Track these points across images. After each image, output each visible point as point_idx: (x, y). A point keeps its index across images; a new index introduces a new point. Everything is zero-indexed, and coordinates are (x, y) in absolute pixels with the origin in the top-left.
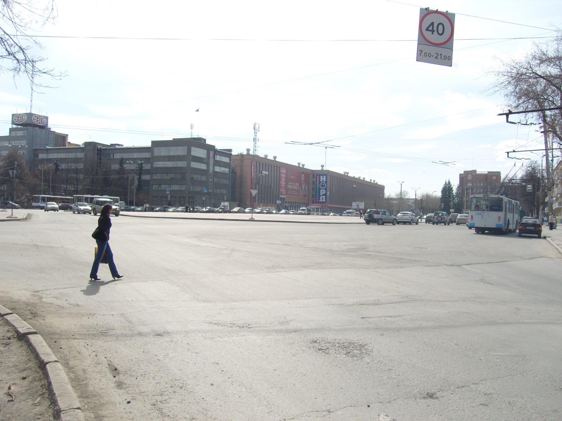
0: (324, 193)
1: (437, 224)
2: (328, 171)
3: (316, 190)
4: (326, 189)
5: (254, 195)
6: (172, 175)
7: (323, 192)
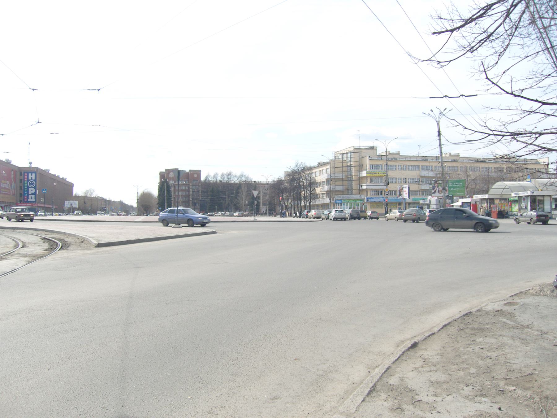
0: (34, 191)
1: (418, 222)
3: (24, 188)
4: (35, 188)
5: (255, 196)
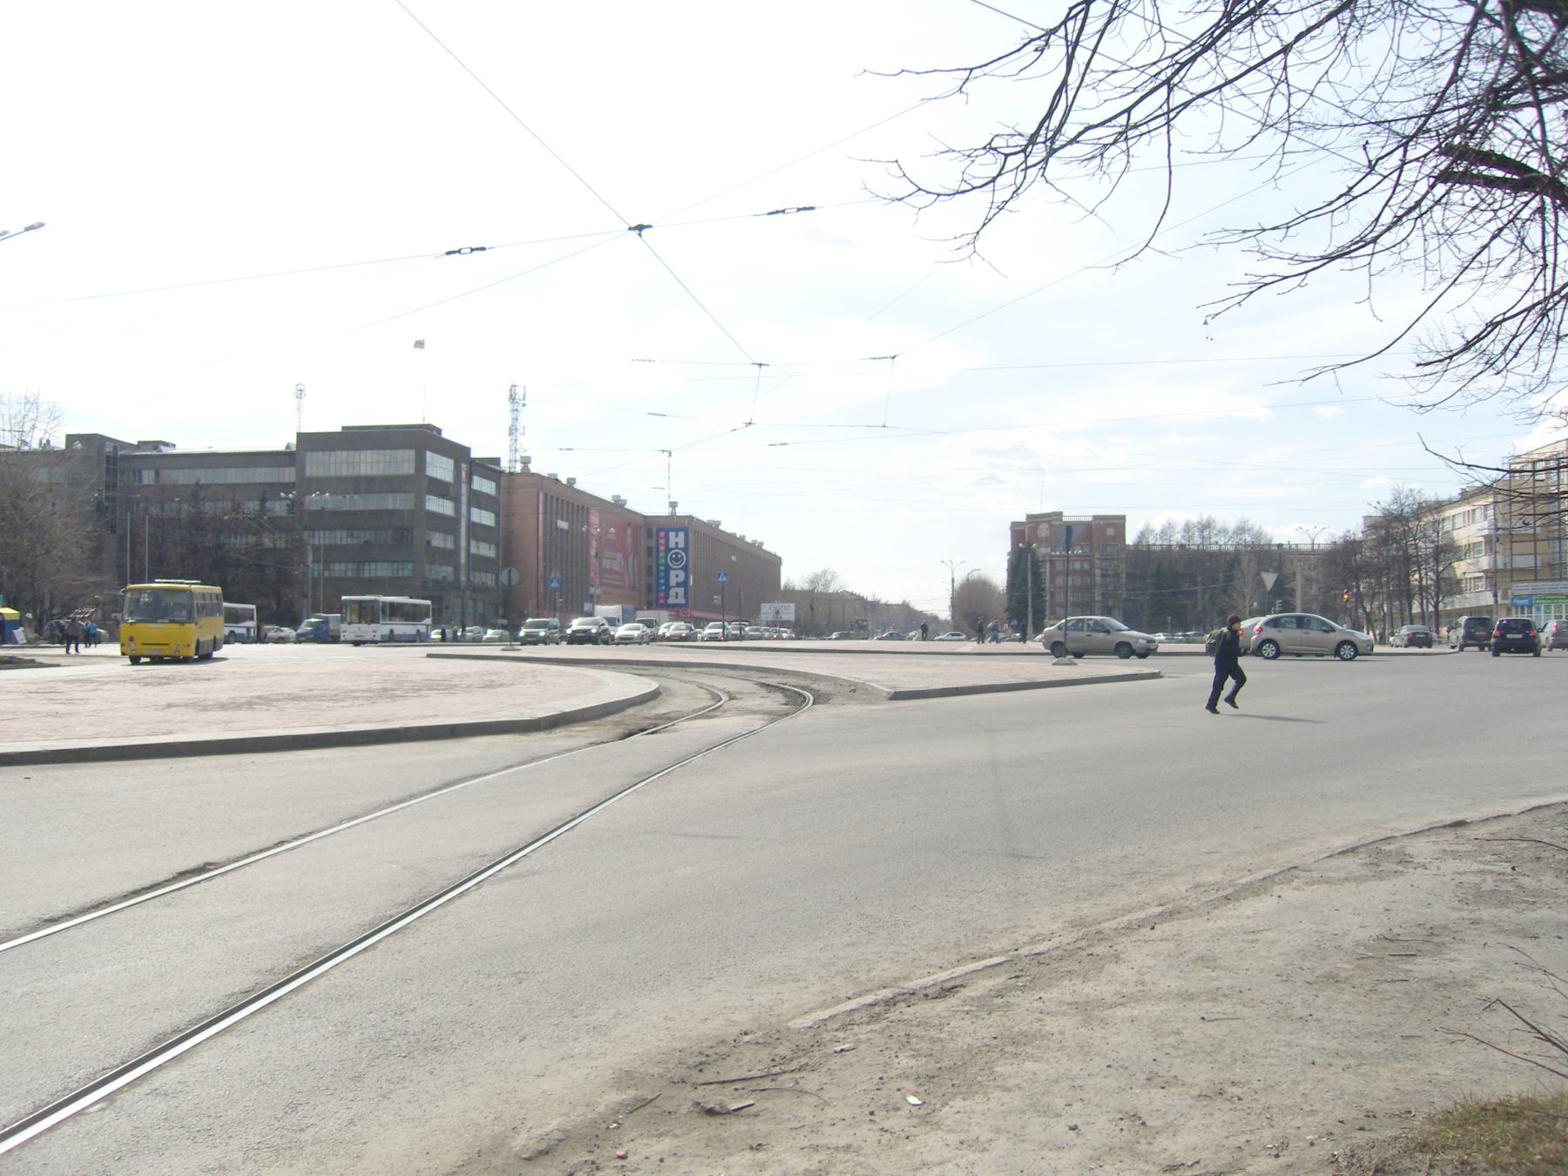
2: (690, 518)
4: (685, 569)
6: (368, 535)
7: (676, 576)
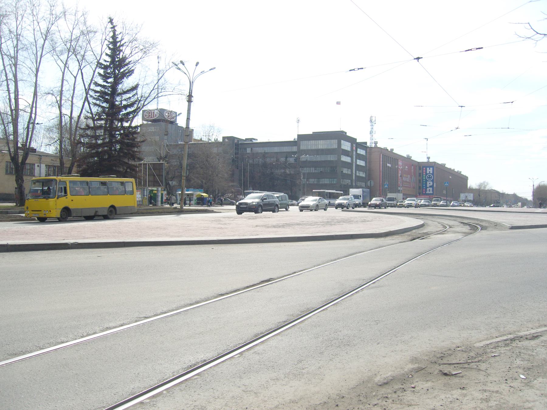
1: (336, 208)
2: (435, 163)
3: (423, 182)
4: (433, 181)
6: (322, 169)
7: (430, 183)
